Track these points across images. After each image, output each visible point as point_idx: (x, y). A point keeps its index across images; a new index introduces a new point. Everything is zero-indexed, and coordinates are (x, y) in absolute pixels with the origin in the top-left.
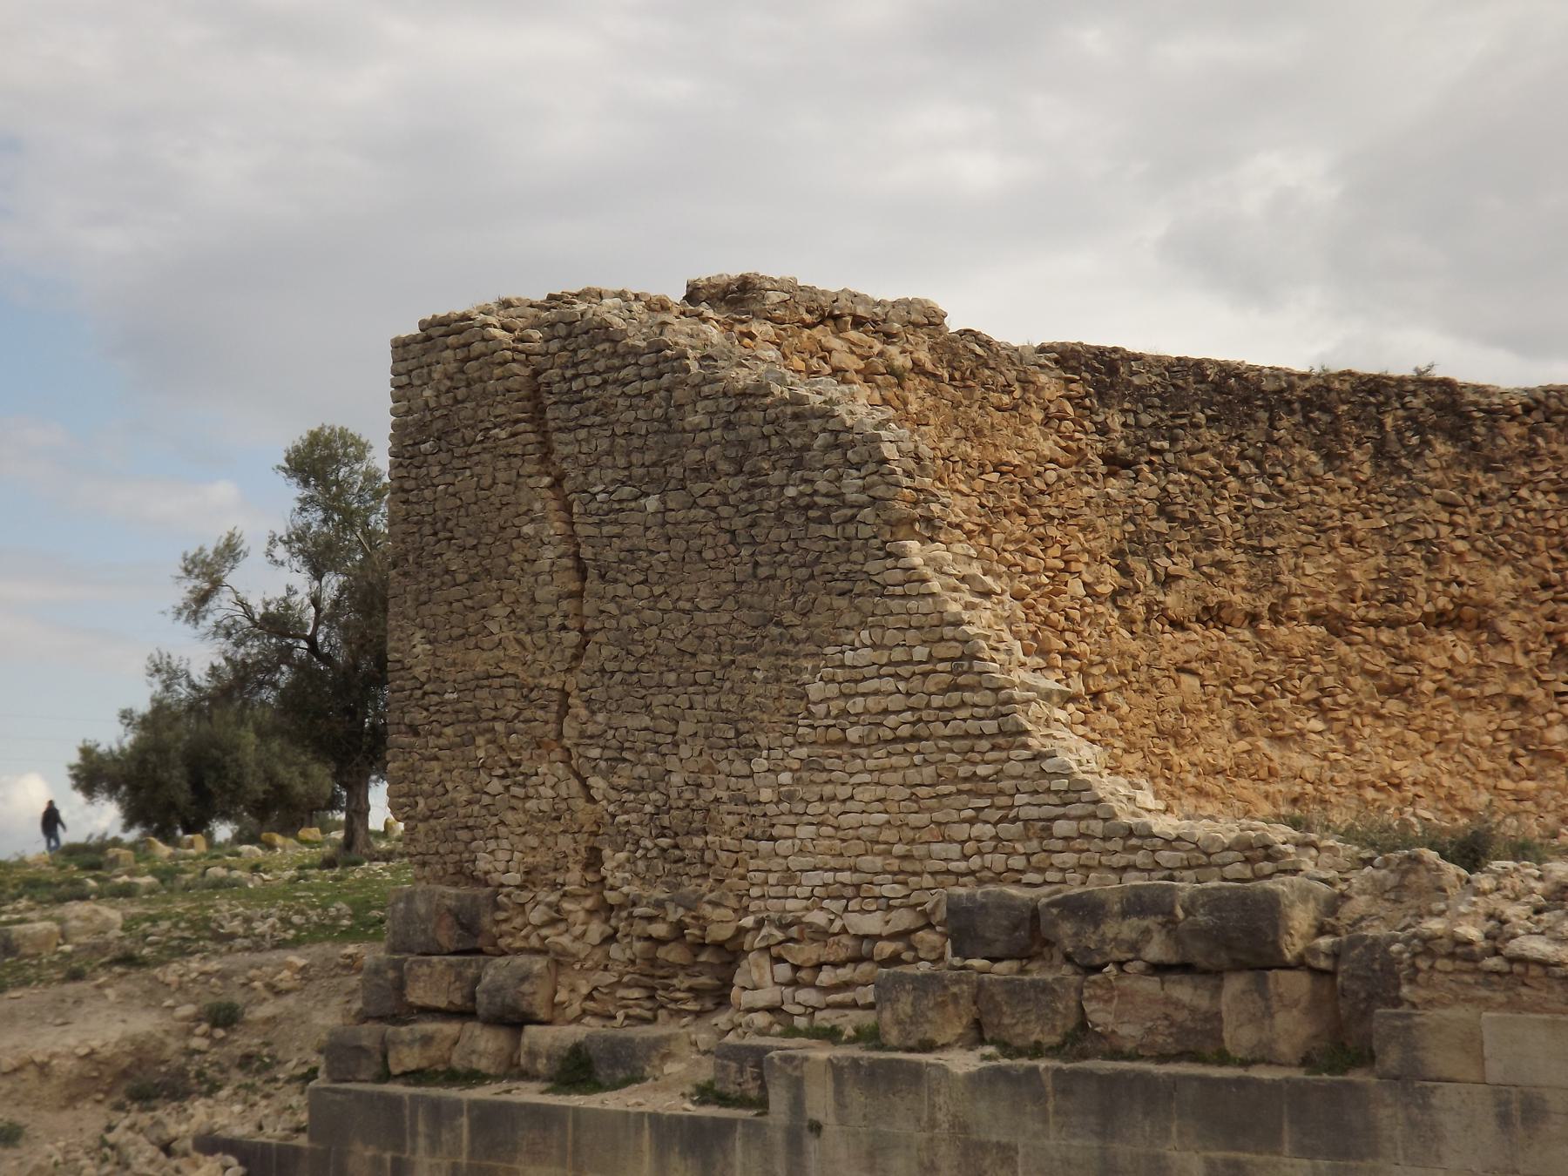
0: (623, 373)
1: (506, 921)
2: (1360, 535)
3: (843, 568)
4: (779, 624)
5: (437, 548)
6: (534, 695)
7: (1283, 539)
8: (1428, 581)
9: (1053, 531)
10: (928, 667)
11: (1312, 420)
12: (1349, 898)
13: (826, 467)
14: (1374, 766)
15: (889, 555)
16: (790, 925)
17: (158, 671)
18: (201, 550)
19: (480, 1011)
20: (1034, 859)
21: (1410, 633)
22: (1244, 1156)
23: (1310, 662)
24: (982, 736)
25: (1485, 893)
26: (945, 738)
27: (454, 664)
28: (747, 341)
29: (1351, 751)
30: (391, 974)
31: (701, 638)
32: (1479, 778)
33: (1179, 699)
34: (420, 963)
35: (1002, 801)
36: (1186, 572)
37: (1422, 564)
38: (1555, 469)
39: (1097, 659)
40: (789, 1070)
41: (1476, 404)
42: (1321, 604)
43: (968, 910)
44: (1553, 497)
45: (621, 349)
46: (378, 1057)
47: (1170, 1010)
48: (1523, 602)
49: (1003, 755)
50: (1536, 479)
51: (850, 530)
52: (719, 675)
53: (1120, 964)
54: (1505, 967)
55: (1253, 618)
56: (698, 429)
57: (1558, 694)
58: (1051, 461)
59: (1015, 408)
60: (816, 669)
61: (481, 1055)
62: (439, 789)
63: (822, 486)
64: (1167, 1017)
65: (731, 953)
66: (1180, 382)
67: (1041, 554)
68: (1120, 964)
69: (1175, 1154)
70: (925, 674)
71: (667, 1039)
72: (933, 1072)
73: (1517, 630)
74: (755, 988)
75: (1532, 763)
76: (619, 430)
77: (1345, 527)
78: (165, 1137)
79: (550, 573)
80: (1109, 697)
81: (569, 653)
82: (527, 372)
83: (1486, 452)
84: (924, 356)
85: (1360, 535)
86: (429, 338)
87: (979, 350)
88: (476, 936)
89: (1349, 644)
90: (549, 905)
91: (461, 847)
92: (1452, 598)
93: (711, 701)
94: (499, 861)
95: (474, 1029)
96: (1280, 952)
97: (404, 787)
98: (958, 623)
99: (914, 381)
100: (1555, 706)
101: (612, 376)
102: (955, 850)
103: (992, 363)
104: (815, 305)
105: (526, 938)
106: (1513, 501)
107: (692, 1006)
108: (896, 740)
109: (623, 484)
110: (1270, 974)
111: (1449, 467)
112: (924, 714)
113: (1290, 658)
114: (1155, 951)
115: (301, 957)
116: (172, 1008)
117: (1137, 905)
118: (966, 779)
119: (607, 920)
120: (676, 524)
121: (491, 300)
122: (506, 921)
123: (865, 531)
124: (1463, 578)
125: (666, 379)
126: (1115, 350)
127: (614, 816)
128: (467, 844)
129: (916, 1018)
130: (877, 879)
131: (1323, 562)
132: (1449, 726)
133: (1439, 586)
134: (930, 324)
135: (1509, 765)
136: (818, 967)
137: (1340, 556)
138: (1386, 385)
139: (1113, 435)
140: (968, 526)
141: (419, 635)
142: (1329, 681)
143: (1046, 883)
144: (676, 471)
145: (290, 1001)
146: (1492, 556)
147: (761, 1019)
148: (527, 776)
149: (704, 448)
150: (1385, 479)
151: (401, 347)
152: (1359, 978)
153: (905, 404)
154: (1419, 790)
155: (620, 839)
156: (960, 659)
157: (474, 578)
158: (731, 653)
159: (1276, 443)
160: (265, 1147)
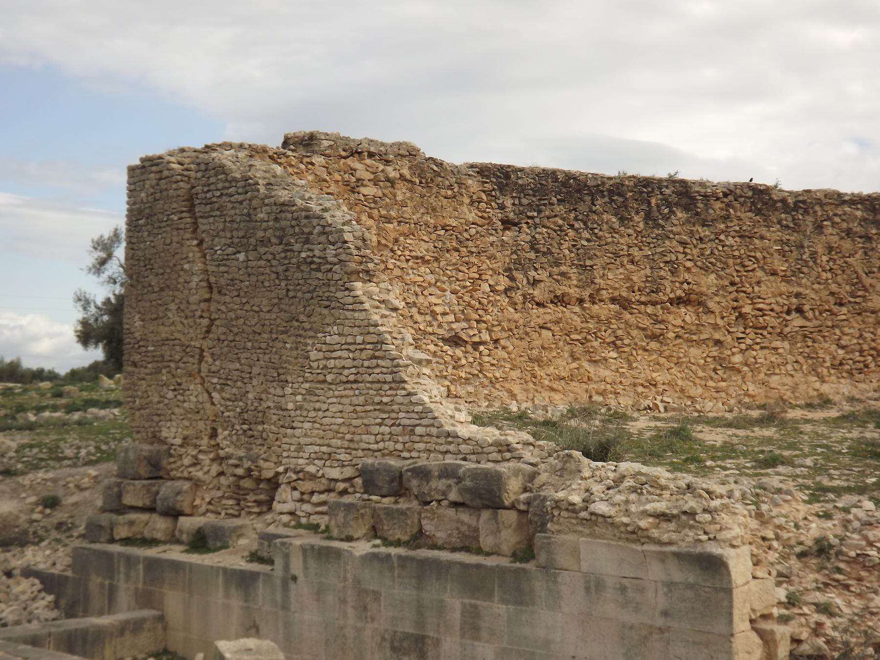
0: (230, 190)
1: (174, 462)
2: (636, 259)
3: (327, 294)
4: (297, 321)
5: (146, 274)
6: (188, 350)
7: (597, 261)
8: (672, 282)
9: (473, 259)
10: (363, 346)
11: (613, 201)
12: (539, 474)
13: (319, 243)
14: (642, 375)
15: (347, 289)
16: (299, 472)
17: (80, 300)
18: (102, 237)
19: (158, 509)
20: (407, 445)
21: (662, 308)
22: (478, 602)
23: (610, 322)
24: (385, 382)
25: (586, 479)
26: (369, 382)
27: (152, 332)
28: (310, 166)
29: (631, 368)
30: (116, 489)
31: (263, 325)
32: (697, 381)
33: (541, 342)
34: (129, 484)
35: (393, 415)
36: (545, 279)
37: (669, 273)
38: (739, 225)
39: (496, 323)
40: (284, 549)
41: (698, 192)
42: (616, 294)
43: (371, 472)
44: (737, 239)
45: (229, 179)
46: (108, 531)
47: (459, 525)
48: (721, 292)
49: (394, 392)
50: (729, 230)
51: (330, 275)
52: (271, 344)
53: (439, 501)
54: (588, 517)
55: (581, 301)
56: (262, 221)
57: (738, 338)
58: (473, 224)
59: (454, 197)
60: (313, 344)
61: (158, 531)
62: (145, 395)
63: (317, 253)
64: (458, 529)
65: (274, 484)
66: (544, 182)
67: (467, 271)
68: (439, 501)
69: (449, 600)
70: (362, 350)
71: (241, 527)
72: (346, 554)
73: (718, 306)
74: (284, 503)
75: (725, 373)
76: (228, 219)
77: (629, 255)
78: (9, 568)
79: (196, 289)
80: (502, 342)
81: (204, 329)
82: (189, 186)
83: (702, 217)
84: (406, 172)
85: (636, 259)
86: (143, 167)
87: (435, 168)
88: (159, 470)
89: (631, 314)
90: (193, 456)
91: (155, 424)
92: (684, 290)
93: (267, 357)
94: (172, 433)
95: (155, 517)
96: (502, 501)
97: (130, 393)
98: (376, 325)
99: (400, 185)
100: (736, 344)
101: (225, 192)
102: (372, 438)
103: (442, 175)
104: (347, 147)
105: (182, 472)
106: (717, 241)
107: (256, 510)
108: (348, 382)
109: (230, 246)
110: (500, 511)
111: (684, 224)
112: (360, 370)
113: (600, 321)
114: (453, 496)
115: (95, 470)
116: (25, 498)
117: (447, 473)
118: (378, 404)
119: (220, 464)
120: (252, 268)
121: (175, 146)
122: (174, 462)
123: (336, 277)
124: (690, 280)
125: (249, 194)
126: (509, 166)
127: (223, 413)
128: (158, 423)
129: (345, 524)
130: (338, 451)
131: (618, 273)
132: (681, 355)
133: (677, 285)
134: (410, 155)
135: (713, 374)
136: (312, 493)
137: (627, 269)
138: (652, 183)
139: (507, 210)
140: (427, 258)
141: (137, 317)
142: (620, 333)
143: (411, 457)
144: (252, 241)
145: (87, 494)
146: (705, 269)
147: (285, 518)
148: (184, 390)
149: (265, 230)
150: (650, 230)
151: (132, 170)
152: (538, 515)
153: (395, 196)
154: (665, 387)
155: (225, 424)
156: (377, 343)
157: (162, 289)
158: (276, 333)
159: (594, 212)
160: (52, 575)
